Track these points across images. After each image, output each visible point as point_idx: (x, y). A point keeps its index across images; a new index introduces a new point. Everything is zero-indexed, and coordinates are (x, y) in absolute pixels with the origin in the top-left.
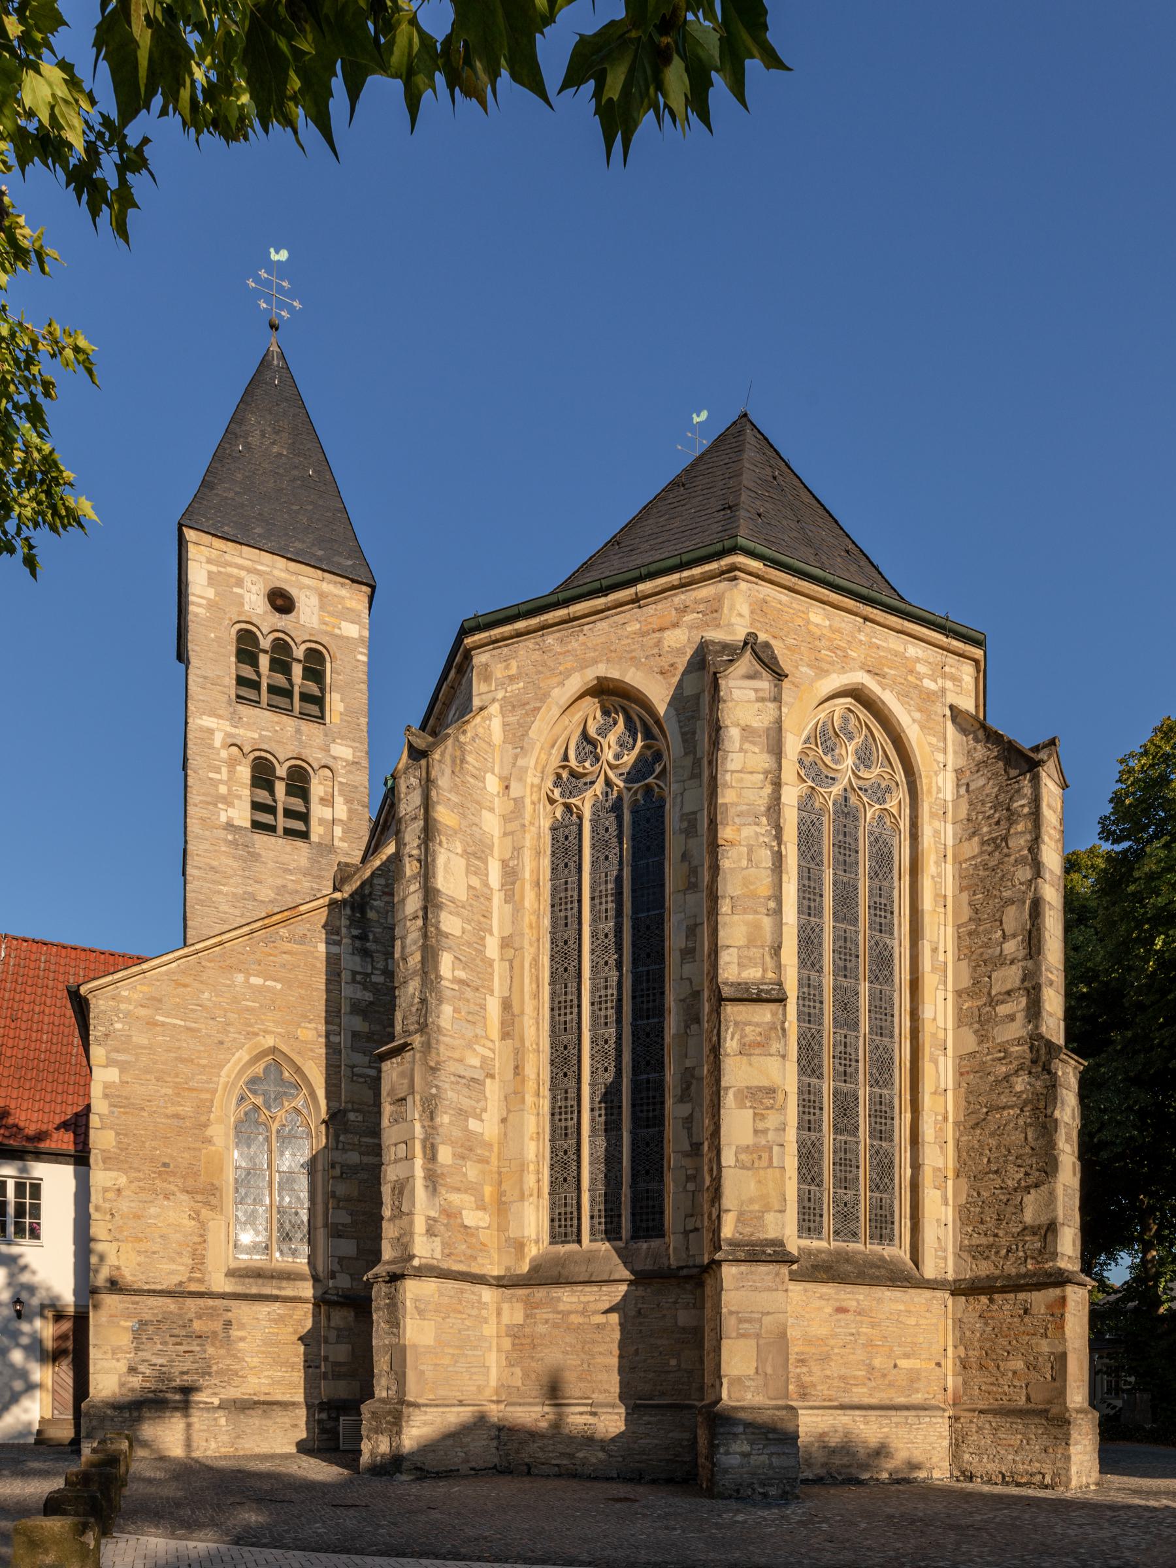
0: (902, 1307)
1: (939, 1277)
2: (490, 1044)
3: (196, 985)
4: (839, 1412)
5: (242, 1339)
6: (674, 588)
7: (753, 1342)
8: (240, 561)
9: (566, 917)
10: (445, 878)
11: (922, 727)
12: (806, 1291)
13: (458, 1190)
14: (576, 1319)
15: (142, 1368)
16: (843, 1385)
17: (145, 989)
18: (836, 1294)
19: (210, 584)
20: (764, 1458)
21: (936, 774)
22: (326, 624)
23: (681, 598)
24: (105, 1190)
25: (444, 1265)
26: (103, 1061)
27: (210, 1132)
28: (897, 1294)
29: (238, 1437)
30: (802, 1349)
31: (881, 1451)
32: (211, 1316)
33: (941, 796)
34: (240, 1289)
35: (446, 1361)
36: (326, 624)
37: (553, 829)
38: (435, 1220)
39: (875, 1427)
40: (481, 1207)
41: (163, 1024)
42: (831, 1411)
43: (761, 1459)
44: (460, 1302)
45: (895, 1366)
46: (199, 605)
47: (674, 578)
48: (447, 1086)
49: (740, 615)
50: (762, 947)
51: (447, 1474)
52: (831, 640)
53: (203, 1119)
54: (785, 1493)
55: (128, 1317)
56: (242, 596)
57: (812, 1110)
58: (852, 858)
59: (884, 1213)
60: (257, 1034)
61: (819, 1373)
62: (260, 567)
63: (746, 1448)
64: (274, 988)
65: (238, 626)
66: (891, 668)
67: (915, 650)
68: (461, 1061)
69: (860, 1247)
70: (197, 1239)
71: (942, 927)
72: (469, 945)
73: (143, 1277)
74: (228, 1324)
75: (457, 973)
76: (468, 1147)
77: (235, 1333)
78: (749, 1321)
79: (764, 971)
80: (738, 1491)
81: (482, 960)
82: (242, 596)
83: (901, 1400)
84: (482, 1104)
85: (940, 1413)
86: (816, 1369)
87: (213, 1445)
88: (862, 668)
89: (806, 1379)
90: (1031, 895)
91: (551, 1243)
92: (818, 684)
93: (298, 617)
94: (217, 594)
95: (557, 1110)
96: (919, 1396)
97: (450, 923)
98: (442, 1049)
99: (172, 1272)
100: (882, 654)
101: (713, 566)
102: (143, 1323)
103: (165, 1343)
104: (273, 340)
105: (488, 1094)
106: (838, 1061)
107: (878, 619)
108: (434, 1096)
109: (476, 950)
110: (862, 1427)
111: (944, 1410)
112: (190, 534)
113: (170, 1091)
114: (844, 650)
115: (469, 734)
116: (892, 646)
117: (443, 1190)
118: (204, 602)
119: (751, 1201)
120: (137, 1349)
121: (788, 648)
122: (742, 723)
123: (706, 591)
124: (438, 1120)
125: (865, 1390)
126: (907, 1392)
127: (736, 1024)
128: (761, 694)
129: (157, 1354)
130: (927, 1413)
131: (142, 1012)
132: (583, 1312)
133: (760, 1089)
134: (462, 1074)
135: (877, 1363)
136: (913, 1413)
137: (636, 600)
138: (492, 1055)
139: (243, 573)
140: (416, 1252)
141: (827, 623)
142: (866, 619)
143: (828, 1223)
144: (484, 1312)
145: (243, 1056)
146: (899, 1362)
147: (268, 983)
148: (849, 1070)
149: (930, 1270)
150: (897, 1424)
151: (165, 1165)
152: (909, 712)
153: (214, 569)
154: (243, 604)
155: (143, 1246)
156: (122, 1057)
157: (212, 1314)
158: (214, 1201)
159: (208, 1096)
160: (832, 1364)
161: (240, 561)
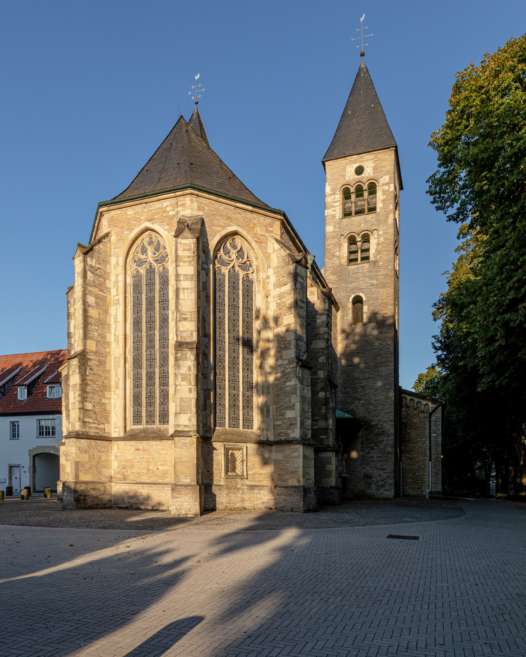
0: (160, 447)
4: (134, 485)
9: (164, 307)
12: (125, 444)
16: (138, 475)
18: (136, 444)
28: (159, 442)
30: (124, 463)
39: (147, 490)
42: (130, 485)
45: (158, 469)
49: (105, 226)
52: (134, 217)
57: (139, 381)
59: (165, 413)
61: (130, 471)
66: (156, 215)
67: (165, 203)
69: (155, 426)
83: (160, 481)
86: (129, 470)
88: (146, 221)
89: (126, 474)
92: (130, 235)
95: (161, 377)
96: (168, 480)
100: (153, 212)
106: (148, 361)
107: (148, 201)
110: (142, 490)
114: (139, 218)
121: (120, 228)
126: (163, 478)
130: (166, 486)
135: (151, 468)
142: (146, 203)
143: (144, 420)
146: (159, 467)
148: (152, 363)
150: (155, 489)
160: (135, 468)
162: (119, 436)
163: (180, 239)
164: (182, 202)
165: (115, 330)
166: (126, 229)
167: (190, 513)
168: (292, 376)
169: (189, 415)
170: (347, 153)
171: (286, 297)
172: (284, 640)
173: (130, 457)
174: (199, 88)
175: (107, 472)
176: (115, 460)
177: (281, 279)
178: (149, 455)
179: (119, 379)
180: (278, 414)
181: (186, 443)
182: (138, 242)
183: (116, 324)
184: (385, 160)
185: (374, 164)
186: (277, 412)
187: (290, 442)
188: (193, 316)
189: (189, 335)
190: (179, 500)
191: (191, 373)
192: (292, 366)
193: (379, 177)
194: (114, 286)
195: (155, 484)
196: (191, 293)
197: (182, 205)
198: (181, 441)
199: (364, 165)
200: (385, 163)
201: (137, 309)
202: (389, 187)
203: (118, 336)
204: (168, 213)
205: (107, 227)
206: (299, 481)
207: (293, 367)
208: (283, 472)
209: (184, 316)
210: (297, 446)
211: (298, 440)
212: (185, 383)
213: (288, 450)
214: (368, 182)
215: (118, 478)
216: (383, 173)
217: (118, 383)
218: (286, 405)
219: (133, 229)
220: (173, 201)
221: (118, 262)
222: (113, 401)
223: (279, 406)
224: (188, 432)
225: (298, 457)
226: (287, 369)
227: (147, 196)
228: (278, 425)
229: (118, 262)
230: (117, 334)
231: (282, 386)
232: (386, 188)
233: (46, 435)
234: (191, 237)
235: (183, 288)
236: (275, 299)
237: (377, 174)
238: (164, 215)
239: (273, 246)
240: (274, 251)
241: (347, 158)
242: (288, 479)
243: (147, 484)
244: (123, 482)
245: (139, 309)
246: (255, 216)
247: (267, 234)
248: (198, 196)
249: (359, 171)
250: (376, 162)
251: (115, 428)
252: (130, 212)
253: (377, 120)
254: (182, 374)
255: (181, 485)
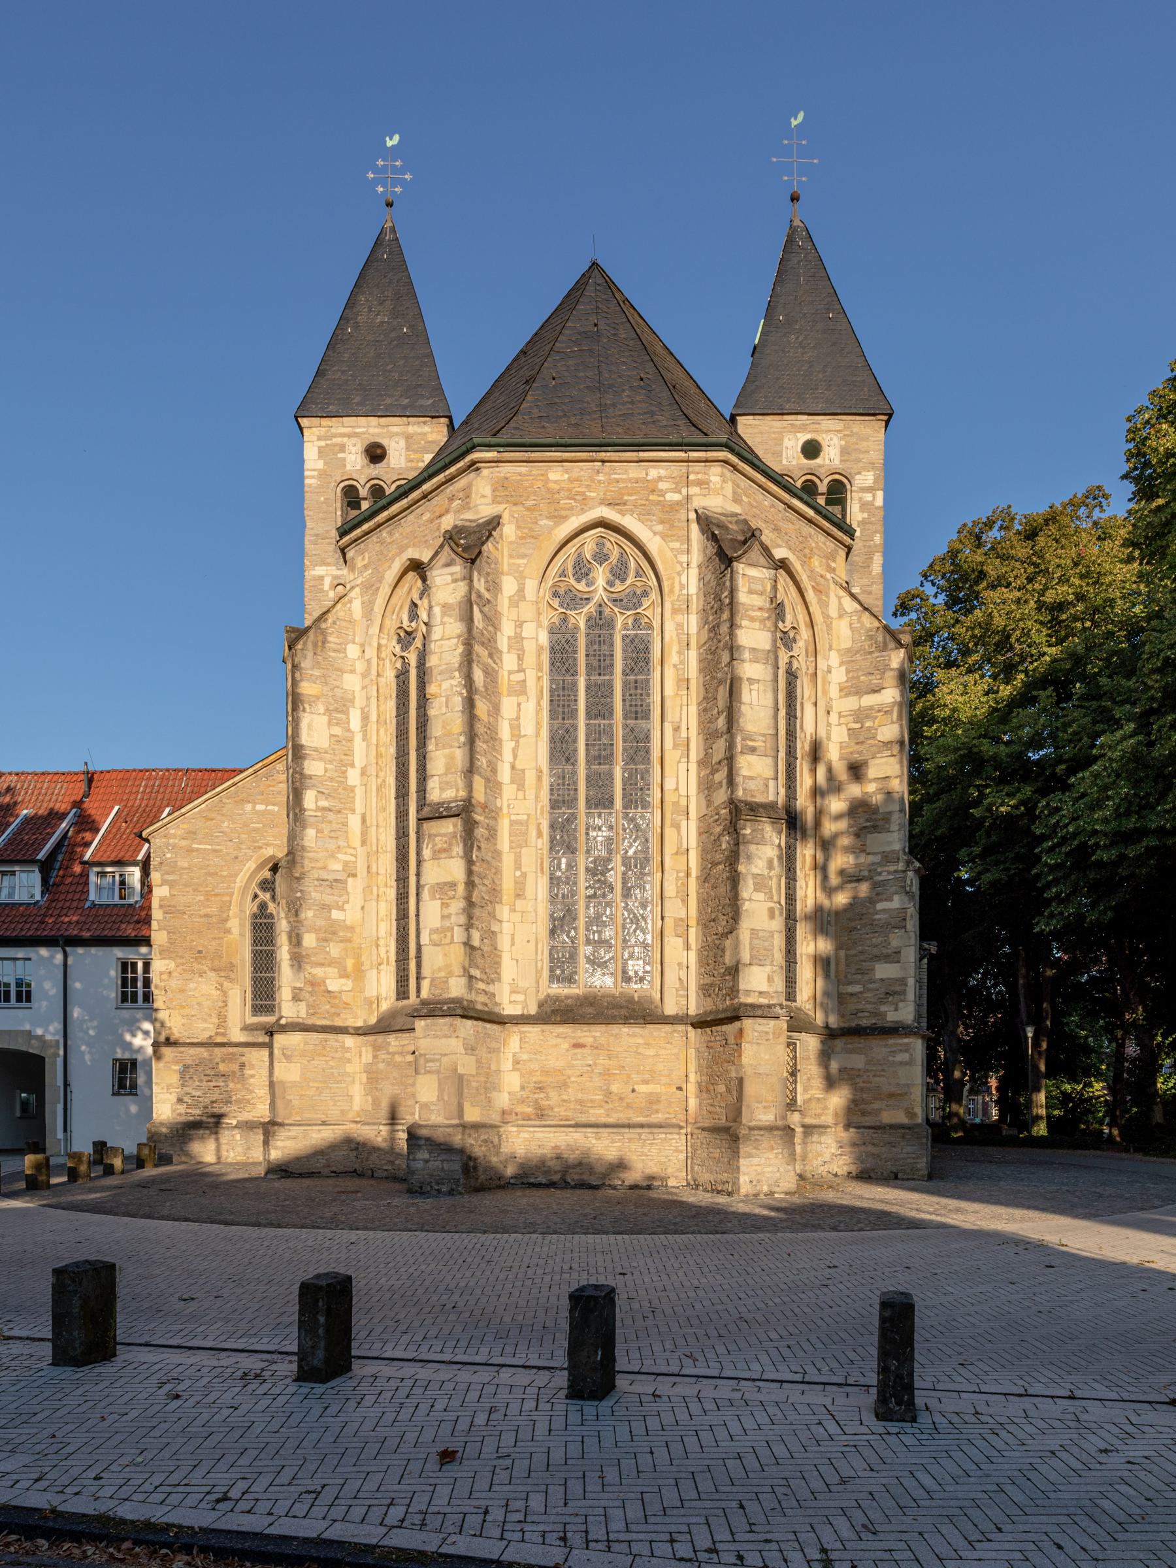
0: (641, 1041)
1: (680, 1013)
2: (352, 851)
3: (219, 817)
5: (252, 1076)
6: (443, 483)
7: (435, 1077)
8: (342, 430)
10: (308, 734)
11: (664, 537)
12: (543, 1031)
13: (322, 965)
14: (398, 1058)
15: (186, 1099)
17: (185, 826)
19: (320, 457)
20: (438, 1163)
21: (679, 574)
22: (411, 461)
23: (451, 489)
24: (161, 973)
25: (309, 1022)
26: (159, 882)
27: (229, 925)
28: (636, 1029)
29: (249, 1149)
30: (540, 1078)
31: (621, 1165)
32: (231, 1060)
33: (685, 592)
34: (250, 1039)
35: (311, 1092)
36: (411, 461)
37: (397, 677)
38: (300, 989)
40: (344, 975)
41: (197, 850)
43: (435, 1164)
44: (324, 1048)
45: (633, 1091)
46: (312, 477)
47: (441, 477)
48: (311, 889)
50: (456, 773)
51: (311, 1175)
52: (569, 490)
53: (225, 915)
54: (452, 1190)
55: (177, 1063)
56: (344, 459)
58: (608, 662)
60: (261, 848)
62: (358, 430)
63: (427, 1156)
64: (273, 811)
65: (342, 485)
66: (631, 495)
67: (654, 472)
68: (324, 868)
70: (221, 1004)
71: (685, 708)
72: (331, 779)
73: (186, 1034)
74: (243, 1065)
75: (319, 804)
76: (331, 932)
77: (248, 1072)
78: (432, 1061)
79: (457, 791)
80: (421, 1188)
81: (344, 789)
82: (344, 459)
83: (641, 1119)
84: (345, 898)
85: (676, 1130)
86: (553, 1094)
87: (232, 1154)
89: (544, 1103)
90: (729, 676)
91: (398, 999)
92: (556, 531)
93: (388, 464)
94: (325, 464)
96: (660, 1115)
97: (313, 767)
98: (306, 862)
99: (204, 1029)
100: (621, 485)
101: (461, 464)
102: (186, 1067)
103: (200, 1081)
104: (388, 217)
105: (349, 889)
108: (299, 898)
109: (338, 782)
110: (594, 1141)
111: (681, 1127)
112: (304, 422)
113: (202, 898)
114: (583, 494)
115: (330, 621)
116: (631, 475)
117: (308, 967)
118: (315, 473)
119: (440, 970)
120: (183, 1085)
121: (528, 509)
122: (442, 602)
123: (462, 482)
124: (302, 916)
125: (602, 1111)
127: (430, 836)
128: (455, 577)
129: (197, 1088)
130: (661, 1130)
131: (184, 843)
132: (401, 1053)
133: (445, 884)
134: (325, 877)
135: (614, 1088)
136: (646, 1130)
137: (425, 496)
138: (353, 859)
139: (345, 440)
140: (283, 1014)
141: (566, 476)
142: (603, 461)
144: (348, 1055)
145: (251, 865)
146: (636, 1087)
147: (270, 808)
149: (670, 1009)
150: (630, 1140)
151: (200, 952)
152: (650, 528)
153: (323, 443)
154: (345, 466)
155: (185, 1011)
156: (171, 877)
157: (231, 1058)
158: (232, 975)
159: (228, 898)
161: (342, 430)
162: (525, 1012)
163: (742, 566)
164: (700, 476)
165: (515, 757)
166: (545, 513)
167: (777, 1189)
168: (893, 889)
169: (768, 969)
170: (788, 407)
171: (876, 718)
172: (295, 1482)
173: (554, 1063)
174: (395, 170)
175: (503, 1100)
176: (514, 1070)
177: (862, 678)
178: (610, 1059)
179: (524, 875)
180: (853, 970)
181: (767, 1033)
182: (571, 549)
183: (517, 742)
184: (866, 439)
185: (843, 443)
186: (847, 965)
187: (894, 1030)
188: (768, 745)
189: (762, 788)
190: (755, 1160)
191: (772, 873)
192: (892, 868)
193: (853, 471)
194: (510, 647)
195: (629, 1126)
196: (765, 691)
197: (699, 483)
198: (757, 1027)
199: (823, 439)
200: (865, 444)
201: (560, 709)
202: (874, 496)
203: (523, 771)
204: (663, 496)
205: (489, 500)
206: (910, 1114)
207: (896, 871)
208: (865, 1096)
209: (750, 743)
210: (906, 1040)
211: (908, 1027)
212: (760, 896)
213: (879, 1048)
214: (830, 478)
215: (522, 1113)
216: (861, 464)
217: (524, 884)
218: (875, 951)
219: (566, 518)
220: (677, 470)
221: (521, 590)
222: (506, 927)
223: (853, 952)
224: (769, 1006)
225: (909, 1063)
226: (880, 874)
227: (609, 445)
228: (852, 994)
229: (521, 590)
230: (519, 766)
231: (864, 911)
232: (868, 497)
233: (19, 999)
234: (766, 564)
235: (748, 679)
236: (843, 720)
237: (848, 464)
238: (651, 497)
239: (840, 603)
240: (842, 614)
241: (786, 417)
242: (880, 1110)
243: (606, 1126)
244: (538, 1123)
245: (566, 710)
246: (813, 532)
247: (828, 576)
248: (735, 468)
249: (811, 450)
250: (848, 439)
251: (513, 992)
252: (556, 474)
253: (843, 349)
254: (755, 876)
255: (760, 1128)
